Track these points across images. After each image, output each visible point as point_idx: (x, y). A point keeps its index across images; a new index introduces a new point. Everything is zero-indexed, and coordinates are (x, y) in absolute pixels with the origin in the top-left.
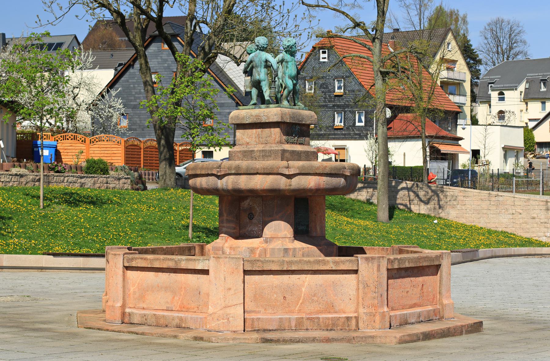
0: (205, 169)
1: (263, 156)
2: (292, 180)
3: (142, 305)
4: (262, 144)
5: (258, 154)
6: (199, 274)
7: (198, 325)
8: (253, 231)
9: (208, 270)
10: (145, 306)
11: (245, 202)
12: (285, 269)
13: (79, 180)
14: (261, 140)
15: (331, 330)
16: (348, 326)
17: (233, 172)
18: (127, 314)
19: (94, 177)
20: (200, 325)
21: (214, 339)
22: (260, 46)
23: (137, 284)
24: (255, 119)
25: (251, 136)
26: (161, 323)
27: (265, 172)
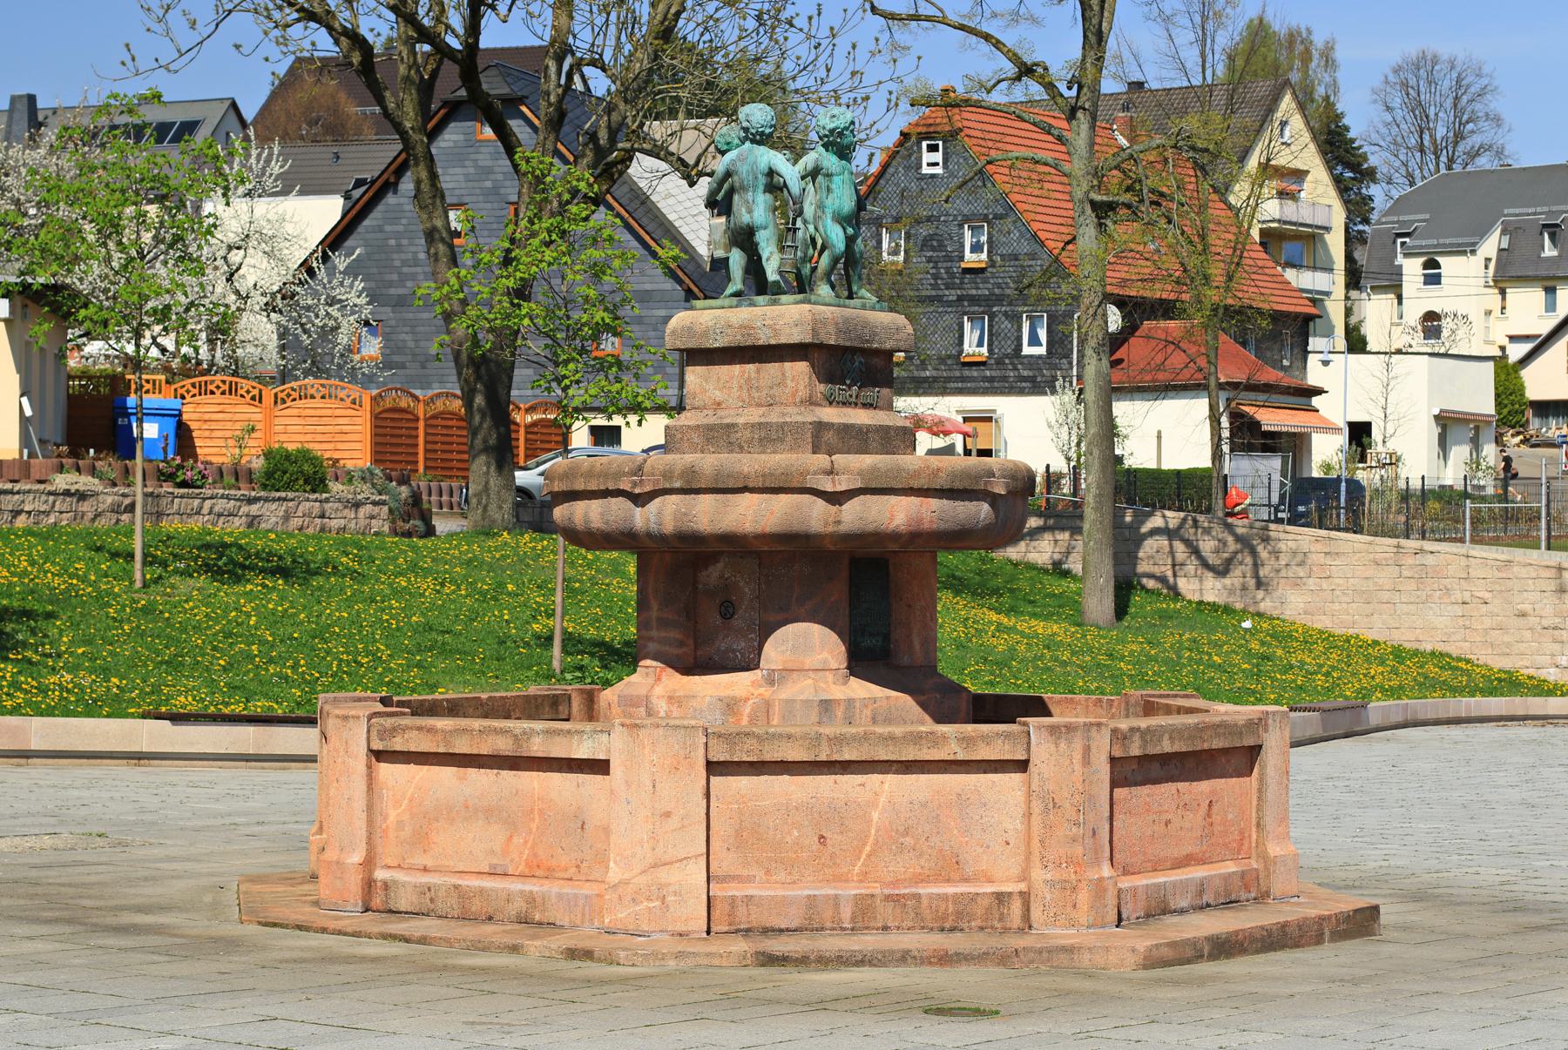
1: (761, 440)
2: (844, 507)
3: (420, 860)
5: (748, 434)
7: (579, 915)
8: (734, 651)
10: (430, 863)
11: (711, 569)
12: (823, 757)
13: (245, 509)
15: (952, 930)
17: (677, 485)
18: (379, 884)
19: (285, 499)
20: (583, 915)
21: (622, 954)
26: (473, 909)
27: (767, 485)
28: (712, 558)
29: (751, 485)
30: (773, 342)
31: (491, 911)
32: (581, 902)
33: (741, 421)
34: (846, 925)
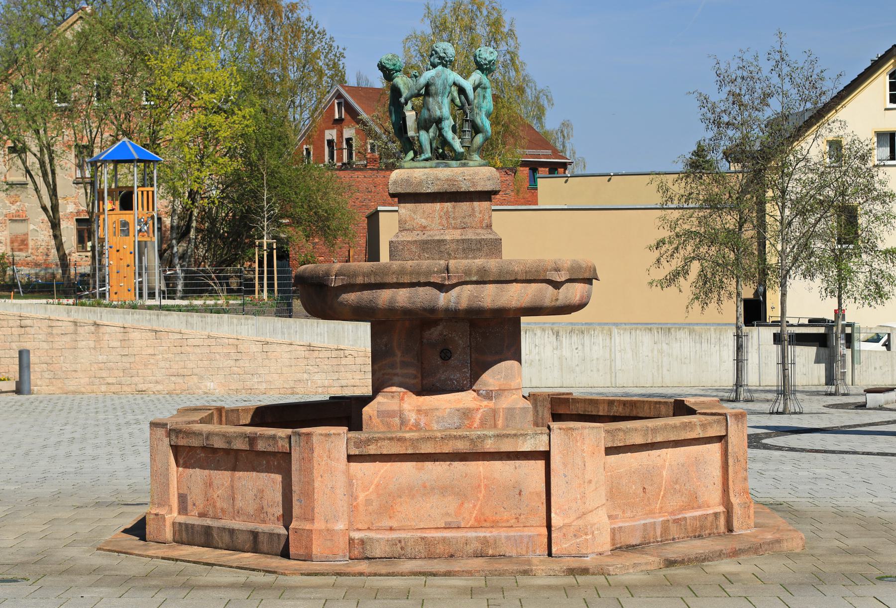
0: (411, 273)
1: (464, 250)
3: (387, 523)
4: (454, 228)
5: (454, 246)
6: (519, 459)
7: (524, 549)
8: (451, 380)
9: (607, 454)
10: (395, 525)
11: (432, 330)
12: (649, 441)
14: (453, 222)
16: (717, 528)
17: (474, 279)
18: (356, 541)
20: (528, 548)
21: (611, 568)
22: (448, 59)
23: (373, 486)
24: (446, 186)
25: (431, 216)
26: (438, 551)
27: (528, 278)
28: (435, 322)
29: (519, 278)
30: (472, 190)
31: (452, 551)
32: (525, 540)
33: (448, 237)
34: (659, 539)
